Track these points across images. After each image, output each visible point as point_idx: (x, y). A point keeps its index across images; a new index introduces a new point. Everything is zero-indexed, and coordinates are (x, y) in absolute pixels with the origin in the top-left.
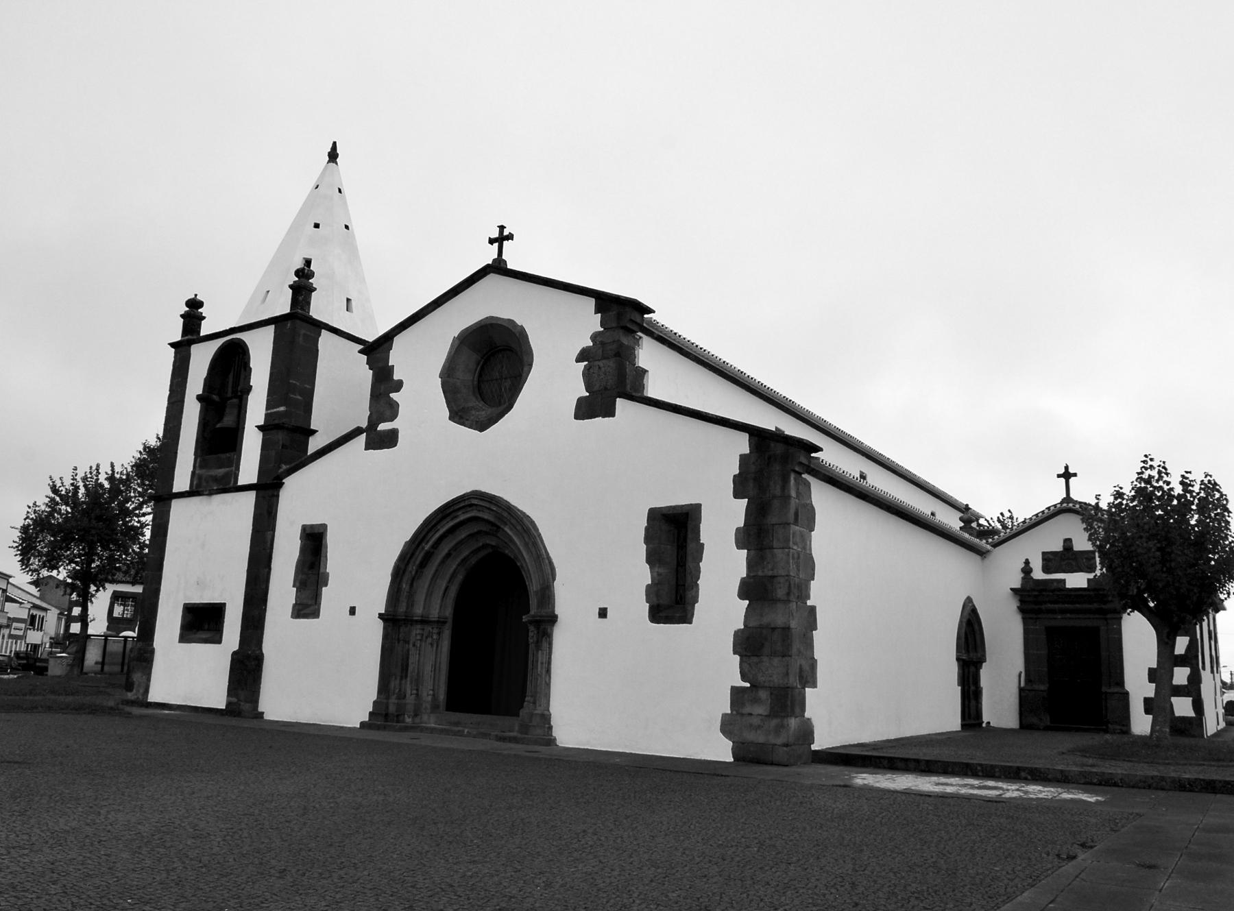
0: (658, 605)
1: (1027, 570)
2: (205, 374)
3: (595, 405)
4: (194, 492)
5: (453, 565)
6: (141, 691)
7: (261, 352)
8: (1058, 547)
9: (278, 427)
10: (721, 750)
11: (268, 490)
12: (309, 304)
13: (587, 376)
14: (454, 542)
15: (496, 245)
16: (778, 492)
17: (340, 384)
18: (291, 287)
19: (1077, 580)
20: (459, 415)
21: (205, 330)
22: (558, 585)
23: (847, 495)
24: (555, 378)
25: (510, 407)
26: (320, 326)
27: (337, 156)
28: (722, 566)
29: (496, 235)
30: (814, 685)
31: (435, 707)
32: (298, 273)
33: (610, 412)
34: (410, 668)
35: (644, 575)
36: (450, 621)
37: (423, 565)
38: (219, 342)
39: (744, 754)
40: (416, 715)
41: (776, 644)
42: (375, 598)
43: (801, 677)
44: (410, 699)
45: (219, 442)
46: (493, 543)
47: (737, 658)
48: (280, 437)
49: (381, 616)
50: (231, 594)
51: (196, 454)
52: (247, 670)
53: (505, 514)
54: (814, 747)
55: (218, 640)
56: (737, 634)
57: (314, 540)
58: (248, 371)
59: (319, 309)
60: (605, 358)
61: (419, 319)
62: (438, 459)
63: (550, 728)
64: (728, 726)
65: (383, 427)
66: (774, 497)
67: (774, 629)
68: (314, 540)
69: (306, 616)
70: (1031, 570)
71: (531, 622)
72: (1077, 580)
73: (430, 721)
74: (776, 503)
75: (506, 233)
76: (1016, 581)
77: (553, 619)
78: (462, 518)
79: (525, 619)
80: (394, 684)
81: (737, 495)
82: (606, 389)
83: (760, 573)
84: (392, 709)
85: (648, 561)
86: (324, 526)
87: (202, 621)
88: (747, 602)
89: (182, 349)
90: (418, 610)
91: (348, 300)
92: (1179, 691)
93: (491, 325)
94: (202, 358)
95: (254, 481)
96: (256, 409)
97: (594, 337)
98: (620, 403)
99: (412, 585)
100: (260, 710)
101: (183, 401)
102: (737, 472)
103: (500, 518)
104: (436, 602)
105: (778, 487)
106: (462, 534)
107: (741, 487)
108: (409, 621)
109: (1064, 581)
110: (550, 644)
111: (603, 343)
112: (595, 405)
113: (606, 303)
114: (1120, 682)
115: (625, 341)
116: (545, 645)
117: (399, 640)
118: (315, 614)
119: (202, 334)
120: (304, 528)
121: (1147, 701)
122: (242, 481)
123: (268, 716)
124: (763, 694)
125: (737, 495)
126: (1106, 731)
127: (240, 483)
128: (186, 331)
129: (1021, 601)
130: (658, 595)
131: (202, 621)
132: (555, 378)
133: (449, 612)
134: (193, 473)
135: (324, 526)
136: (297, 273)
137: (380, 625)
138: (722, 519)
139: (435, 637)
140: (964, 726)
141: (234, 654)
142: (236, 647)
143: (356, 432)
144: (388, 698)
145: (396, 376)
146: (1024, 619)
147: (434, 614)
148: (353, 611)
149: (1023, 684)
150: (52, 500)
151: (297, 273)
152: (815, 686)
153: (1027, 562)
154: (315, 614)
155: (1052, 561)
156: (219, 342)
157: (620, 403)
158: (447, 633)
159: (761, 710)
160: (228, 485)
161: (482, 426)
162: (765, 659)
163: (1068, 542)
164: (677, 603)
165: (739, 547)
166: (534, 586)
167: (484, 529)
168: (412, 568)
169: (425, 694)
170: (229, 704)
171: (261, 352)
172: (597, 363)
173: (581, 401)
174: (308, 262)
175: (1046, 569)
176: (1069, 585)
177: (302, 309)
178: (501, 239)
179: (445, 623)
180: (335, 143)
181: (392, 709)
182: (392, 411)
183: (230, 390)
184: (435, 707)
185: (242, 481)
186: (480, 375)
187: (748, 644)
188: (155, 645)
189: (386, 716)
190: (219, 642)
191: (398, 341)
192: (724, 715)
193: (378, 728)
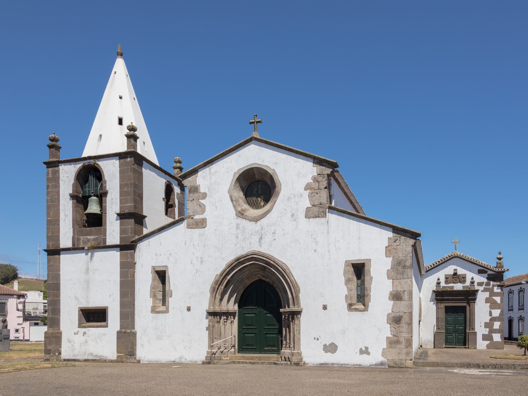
1: (439, 283)
4: (75, 249)
11: (127, 247)
13: (310, 196)
19: (458, 287)
22: (301, 295)
35: (344, 291)
38: (79, 166)
42: (203, 303)
52: (127, 340)
56: (388, 315)
57: (161, 275)
65: (197, 217)
87: (94, 316)
91: (101, 136)
92: (496, 331)
95: (117, 242)
100: (138, 358)
109: (453, 287)
127: (108, 244)
131: (94, 316)
142: (118, 328)
152: (483, 335)
153: (439, 279)
170: (118, 357)
175: (446, 282)
176: (455, 289)
185: (109, 242)
187: (395, 320)
188: (62, 329)
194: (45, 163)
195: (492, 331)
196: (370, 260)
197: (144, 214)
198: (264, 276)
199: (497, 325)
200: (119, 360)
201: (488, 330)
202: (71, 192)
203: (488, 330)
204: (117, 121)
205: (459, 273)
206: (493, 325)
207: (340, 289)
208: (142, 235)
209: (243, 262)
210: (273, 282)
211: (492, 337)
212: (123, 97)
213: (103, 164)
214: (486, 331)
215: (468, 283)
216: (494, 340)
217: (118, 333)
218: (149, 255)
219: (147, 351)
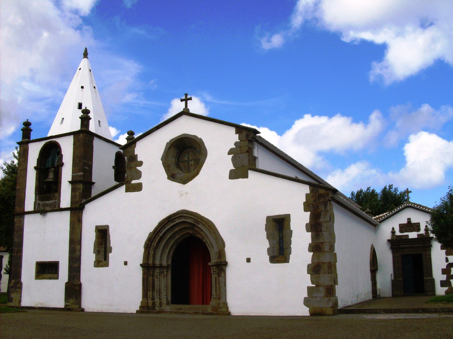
0: (273, 256)
1: (393, 232)
3: (239, 173)
6: (17, 302)
7: (67, 148)
8: (405, 222)
9: (79, 182)
10: (305, 311)
11: (77, 210)
13: (233, 160)
14: (172, 233)
16: (323, 209)
17: (103, 163)
18: (80, 118)
19: (413, 235)
20: (172, 177)
21: (33, 137)
23: (341, 207)
25: (197, 173)
26: (94, 135)
27: (87, 54)
28: (301, 239)
30: (337, 285)
31: (168, 304)
33: (246, 176)
34: (155, 288)
35: (267, 244)
36: (171, 266)
38: (42, 143)
39: (313, 314)
40: (160, 307)
42: (137, 255)
44: (157, 300)
46: (191, 232)
47: (309, 275)
48: (81, 186)
51: (36, 194)
52: (74, 290)
53: (199, 220)
56: (309, 266)
57: (103, 234)
59: (92, 128)
61: (151, 133)
63: (228, 308)
64: (307, 302)
65: (134, 182)
66: (322, 211)
67: (324, 263)
68: (103, 234)
71: (213, 266)
72: (413, 235)
73: (167, 308)
74: (323, 213)
75: (188, 97)
76: (389, 236)
77: (226, 264)
78: (177, 221)
79: (210, 264)
80: (150, 293)
81: (305, 210)
82: (243, 166)
83: (317, 242)
84: (150, 304)
85: (267, 238)
87: (47, 270)
88: (312, 253)
90: (157, 263)
91: (99, 121)
93: (185, 137)
94: (34, 150)
95: (69, 206)
96: (67, 174)
97: (236, 144)
98: (250, 172)
99: (154, 252)
102: (305, 201)
103: (196, 221)
104: (163, 259)
105: (323, 207)
106: (177, 229)
107: (307, 206)
108: (154, 267)
109: (408, 236)
110: (225, 274)
111: (240, 147)
112: (239, 173)
114: (431, 275)
115: (250, 146)
116: (222, 274)
117: (150, 275)
119: (31, 139)
120: (97, 227)
123: (87, 310)
124: (322, 289)
125: (305, 210)
126: (426, 295)
128: (24, 137)
129: (391, 245)
131: (47, 270)
133: (170, 262)
134: (35, 203)
138: (300, 220)
139: (165, 273)
140: (373, 297)
141: (66, 283)
142: (67, 280)
144: (147, 300)
145: (139, 159)
147: (164, 264)
149: (393, 279)
153: (393, 229)
155: (403, 228)
157: (250, 172)
158: (170, 271)
161: (184, 182)
162: (321, 275)
163: (409, 219)
164: (280, 255)
167: (187, 226)
168: (154, 244)
171: (67, 148)
172: (238, 155)
173: (231, 171)
175: (401, 231)
176: (410, 237)
177: (87, 128)
179: (169, 267)
180: (86, 48)
181: (150, 304)
184: (168, 304)
186: (178, 159)
187: (314, 269)
189: (148, 307)
190: (57, 278)
193: (147, 313)
197: (93, 181)
200: (66, 309)
201: (445, 276)
202: (36, 166)
203: (445, 276)
204: (77, 105)
206: (450, 271)
207: (262, 245)
208: (89, 198)
209: (173, 220)
211: (450, 282)
213: (59, 141)
214: (444, 277)
215: (422, 232)
218: (95, 214)
219: (92, 301)
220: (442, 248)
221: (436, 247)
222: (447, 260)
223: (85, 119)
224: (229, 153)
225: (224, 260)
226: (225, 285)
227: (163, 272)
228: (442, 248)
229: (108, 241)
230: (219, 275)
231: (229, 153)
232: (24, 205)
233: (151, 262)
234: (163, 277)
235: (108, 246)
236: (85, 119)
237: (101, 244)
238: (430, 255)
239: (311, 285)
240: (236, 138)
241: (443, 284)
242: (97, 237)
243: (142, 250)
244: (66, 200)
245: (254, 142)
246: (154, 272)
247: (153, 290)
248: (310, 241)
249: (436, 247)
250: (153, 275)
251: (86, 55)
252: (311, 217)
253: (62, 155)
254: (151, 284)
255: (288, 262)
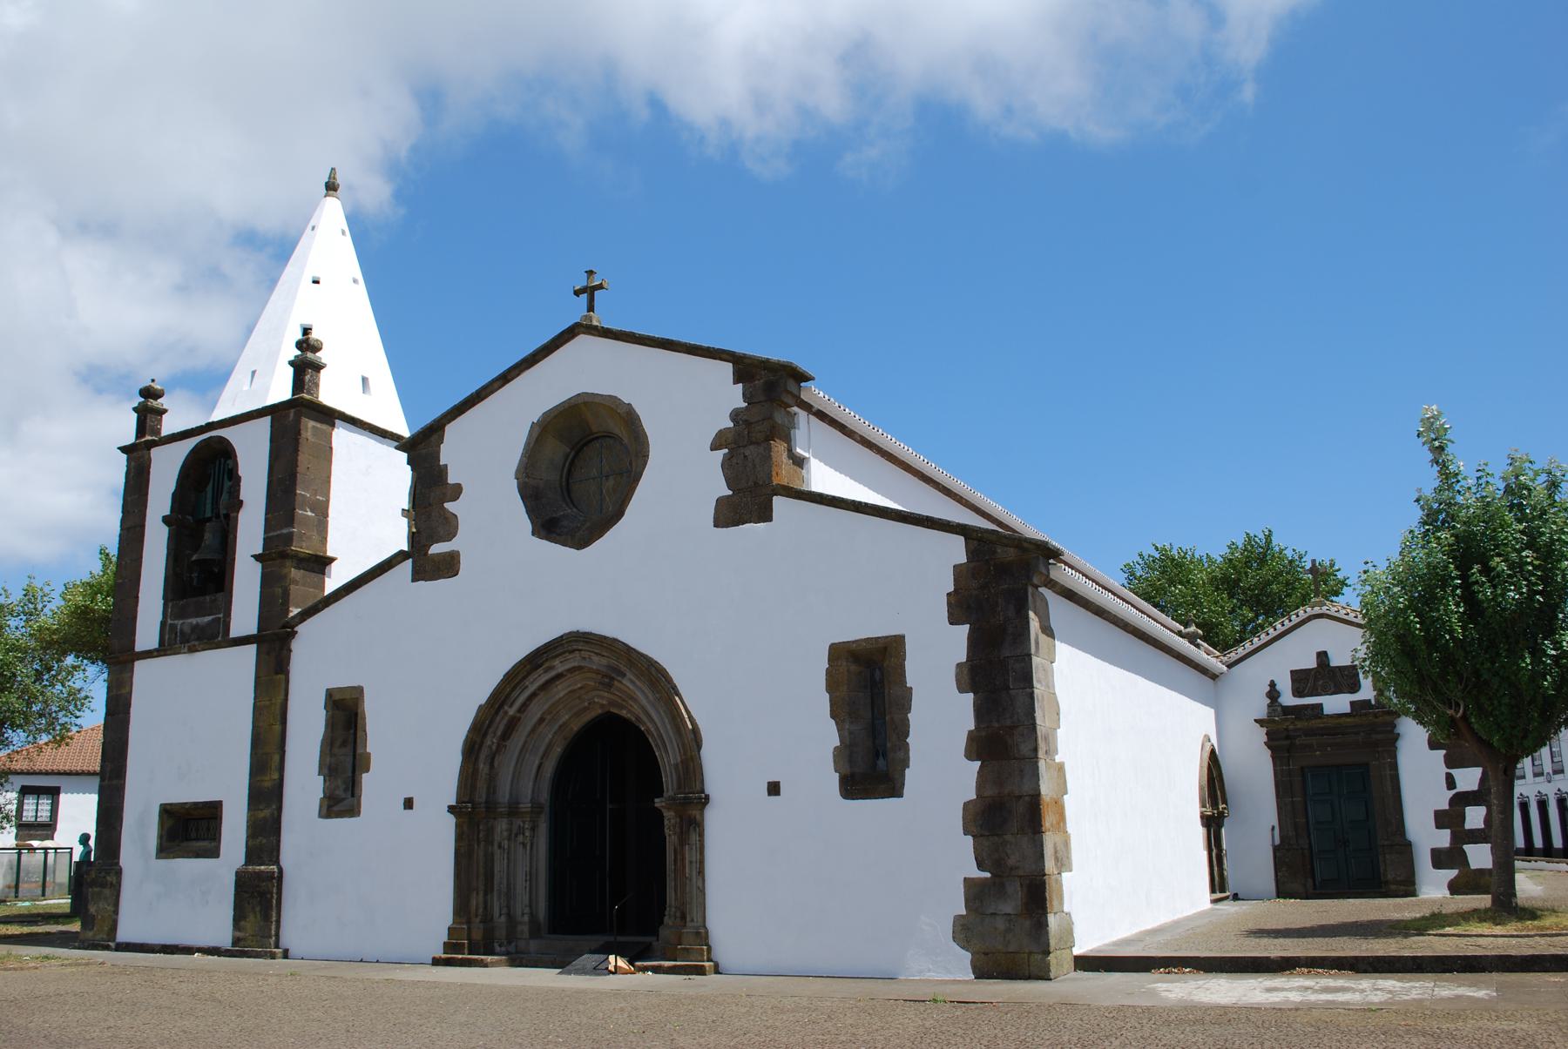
0: (853, 775)
1: (1273, 693)
2: (172, 487)
5: (548, 733)
7: (253, 455)
11: (274, 643)
12: (317, 385)
13: (727, 465)
15: (584, 297)
18: (292, 363)
19: (1336, 704)
21: (169, 426)
24: (682, 470)
26: (331, 417)
28: (940, 718)
29: (582, 282)
31: (535, 932)
32: (300, 345)
33: (765, 515)
35: (829, 736)
36: (547, 809)
37: (506, 736)
38: (192, 443)
40: (509, 943)
41: (1012, 819)
42: (440, 780)
43: (1057, 859)
45: (199, 580)
47: (970, 839)
49: (451, 809)
50: (230, 790)
51: (165, 598)
54: (1077, 951)
55: (214, 853)
57: (345, 713)
58: (235, 479)
59: (331, 391)
60: (752, 443)
62: (527, 589)
65: (436, 549)
68: (345, 713)
69: (340, 815)
70: (1278, 694)
72: (1336, 704)
76: (1261, 707)
80: (476, 901)
81: (954, 620)
86: (359, 690)
87: (189, 828)
88: (979, 763)
89: (138, 457)
91: (365, 380)
92: (1476, 837)
93: (585, 403)
94: (166, 466)
95: (252, 629)
97: (736, 415)
101: (143, 526)
102: (952, 589)
107: (961, 606)
109: (1320, 706)
110: (701, 835)
111: (748, 423)
113: (746, 369)
116: (694, 837)
118: (353, 811)
120: (330, 694)
121: (1434, 851)
122: (235, 632)
130: (851, 761)
132: (682, 470)
134: (163, 624)
135: (359, 690)
136: (299, 345)
137: (451, 820)
138: (936, 656)
143: (399, 557)
145: (452, 479)
146: (1273, 757)
148: (409, 804)
149: (1277, 842)
150: (1445, 581)
151: (299, 345)
153: (1272, 684)
154: (353, 811)
155: (1302, 682)
156: (192, 443)
159: (1008, 907)
160: (216, 636)
162: (1008, 837)
163: (1322, 656)
165: (961, 690)
166: (668, 759)
169: (519, 912)
171: (253, 455)
173: (720, 502)
174: (306, 331)
175: (1297, 693)
176: (1327, 710)
178: (589, 292)
182: (449, 528)
183: (209, 507)
184: (535, 932)
185: (235, 632)
188: (122, 863)
191: (450, 429)
192: (958, 918)
194: (124, 449)
195: (1463, 836)
196: (716, 525)
197: (330, 553)
198: (612, 703)
199: (1475, 817)
201: (1447, 832)
202: (167, 512)
203: (1447, 832)
205: (1336, 661)
210: (638, 719)
212: (317, 275)
214: (1443, 839)
216: (1473, 866)
217: (240, 875)
220: (1433, 745)
221: (1413, 737)
222: (1451, 782)
223: (306, 367)
224: (715, 447)
225: (1026, 788)
226: (701, 872)
227: (521, 831)
228: (1433, 745)
229: (359, 733)
230: (683, 840)
231: (715, 447)
232: (134, 634)
233: (481, 796)
234: (520, 849)
235: (359, 751)
236: (306, 367)
237: (344, 744)
238: (1394, 767)
239: (976, 873)
240: (735, 396)
241: (1440, 859)
242: (331, 724)
243: (456, 760)
244: (245, 614)
245: (795, 409)
246: (490, 831)
247: (489, 889)
248: (971, 725)
249: (1413, 737)
250: (489, 841)
251: (331, 187)
252: (974, 643)
253: (239, 479)
254: (481, 870)
255: (900, 795)
